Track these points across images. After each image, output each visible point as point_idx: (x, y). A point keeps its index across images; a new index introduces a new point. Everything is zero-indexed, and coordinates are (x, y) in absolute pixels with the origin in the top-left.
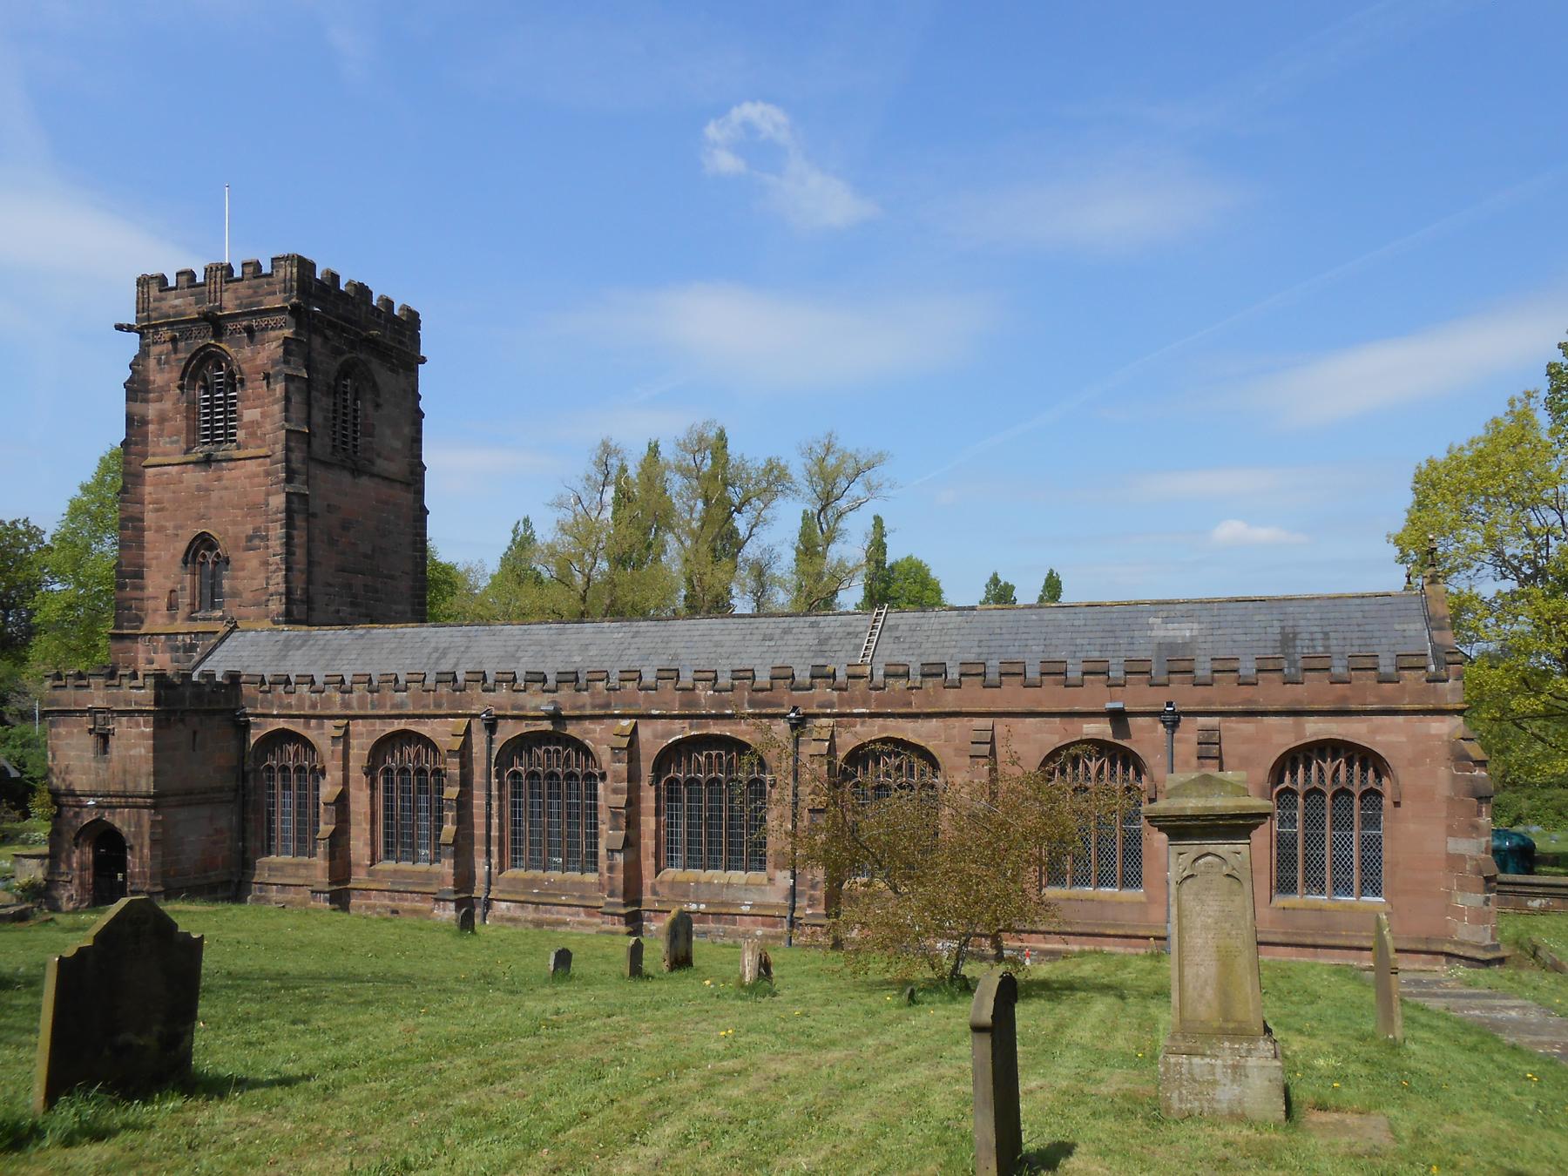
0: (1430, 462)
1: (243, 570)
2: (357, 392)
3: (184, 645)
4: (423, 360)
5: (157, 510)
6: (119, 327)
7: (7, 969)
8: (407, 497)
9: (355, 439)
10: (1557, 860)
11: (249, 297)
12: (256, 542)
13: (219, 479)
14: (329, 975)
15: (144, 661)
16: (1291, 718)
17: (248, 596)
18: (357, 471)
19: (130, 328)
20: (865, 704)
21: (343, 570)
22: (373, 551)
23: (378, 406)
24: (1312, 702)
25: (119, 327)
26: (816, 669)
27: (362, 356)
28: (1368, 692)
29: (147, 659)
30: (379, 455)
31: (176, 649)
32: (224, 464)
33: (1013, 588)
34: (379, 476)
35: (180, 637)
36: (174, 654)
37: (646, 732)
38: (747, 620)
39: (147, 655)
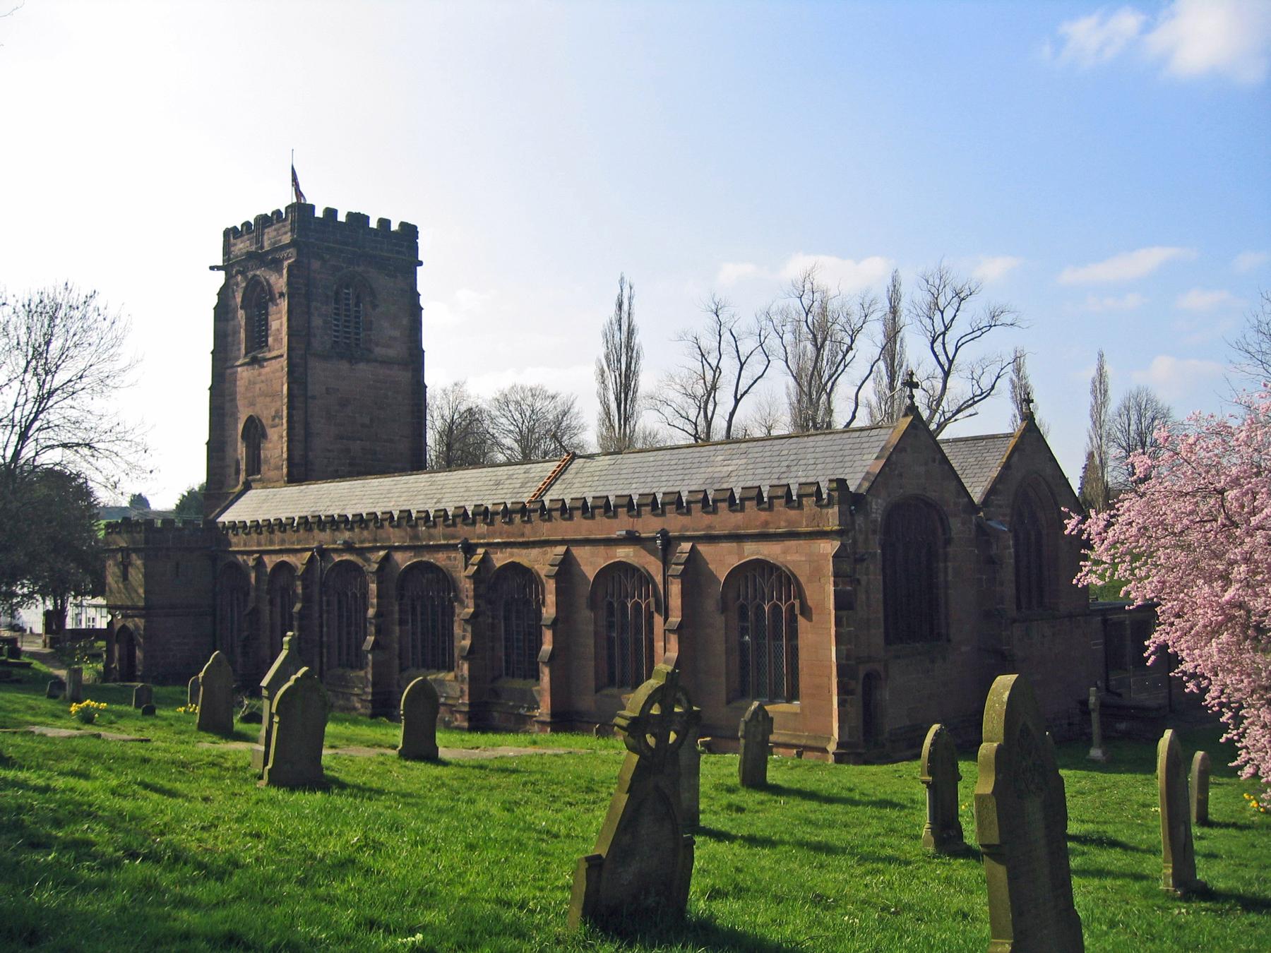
2: (358, 297)
4: (421, 263)
6: (212, 268)
8: (404, 376)
9: (357, 334)
11: (275, 237)
14: (1144, 847)
16: (587, 548)
18: (352, 360)
19: (219, 268)
20: (501, 535)
21: (342, 438)
22: (371, 420)
23: (375, 306)
24: (747, 528)
25: (212, 268)
26: (457, 510)
27: (360, 269)
28: (783, 518)
30: (377, 345)
34: (376, 361)
37: (266, 559)
38: (866, 433)
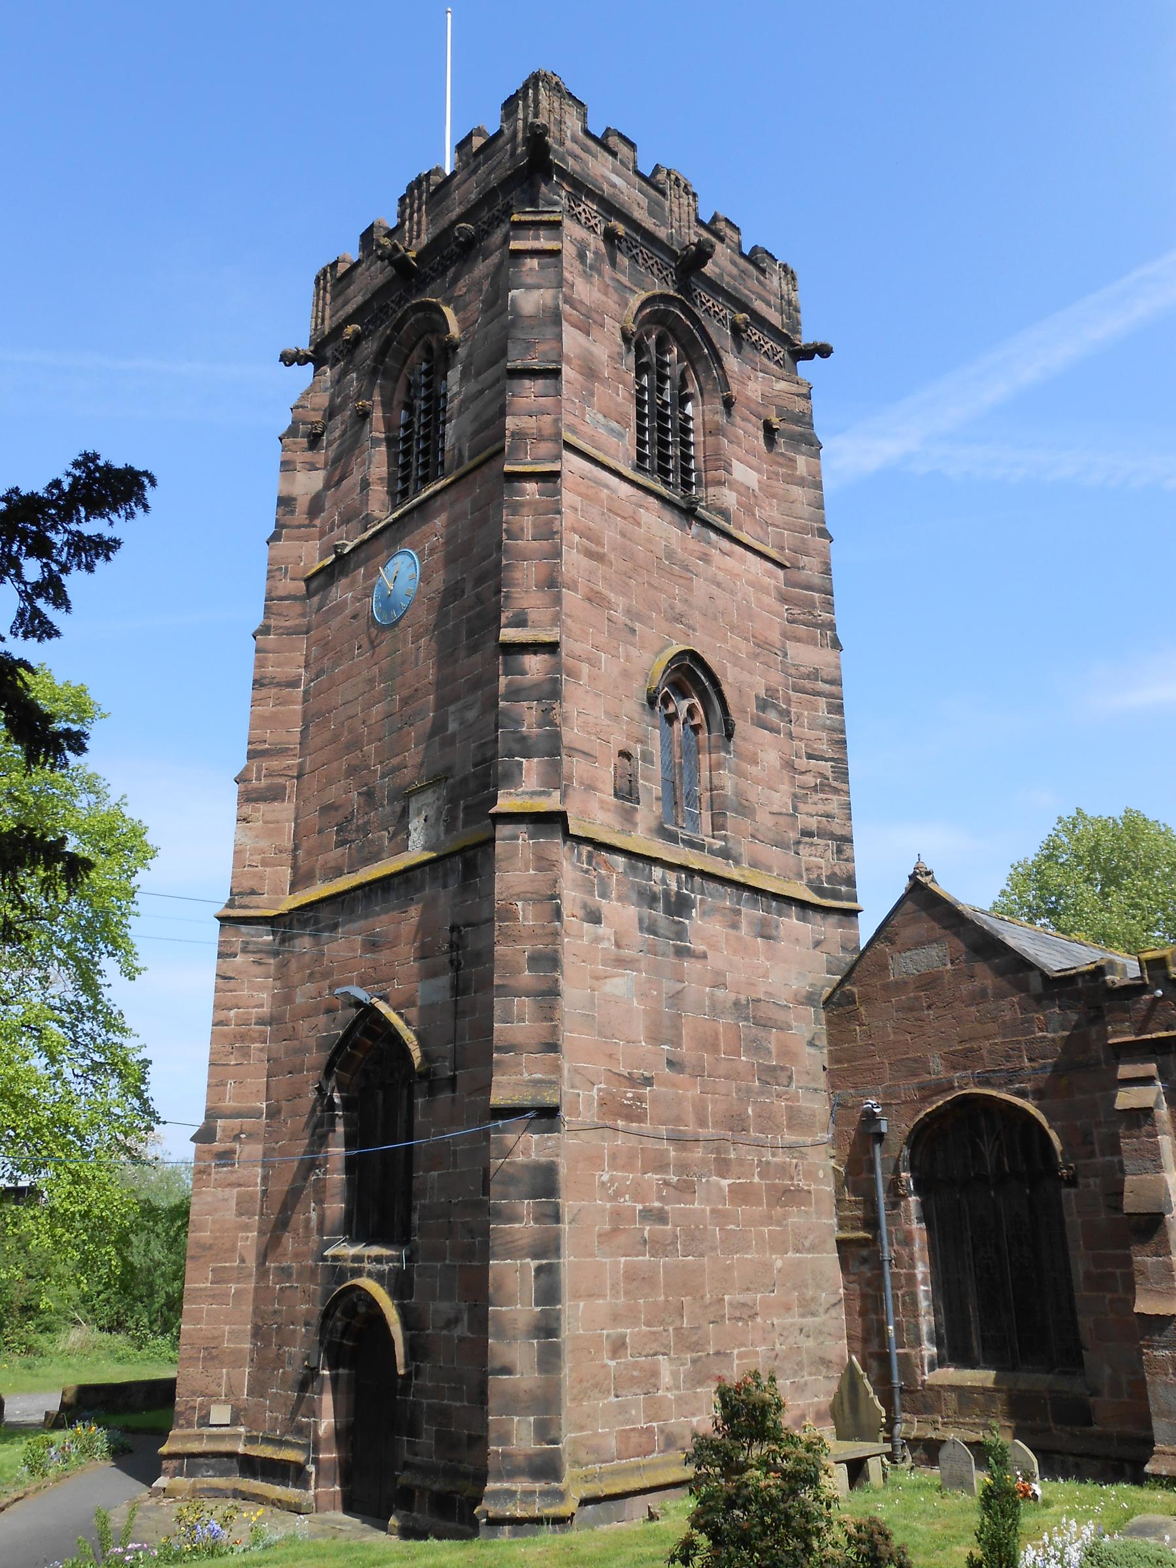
0: (90, 568)
1: (755, 763)
3: (666, 893)
5: (590, 554)
7: (968, 1548)
10: (1001, 1566)
12: (772, 716)
13: (705, 558)
15: (580, 913)
17: (764, 819)
25: (824, 351)
29: (585, 906)
31: (650, 899)
32: (713, 535)
33: (146, 854)
35: (657, 872)
36: (646, 911)
39: (587, 897)
